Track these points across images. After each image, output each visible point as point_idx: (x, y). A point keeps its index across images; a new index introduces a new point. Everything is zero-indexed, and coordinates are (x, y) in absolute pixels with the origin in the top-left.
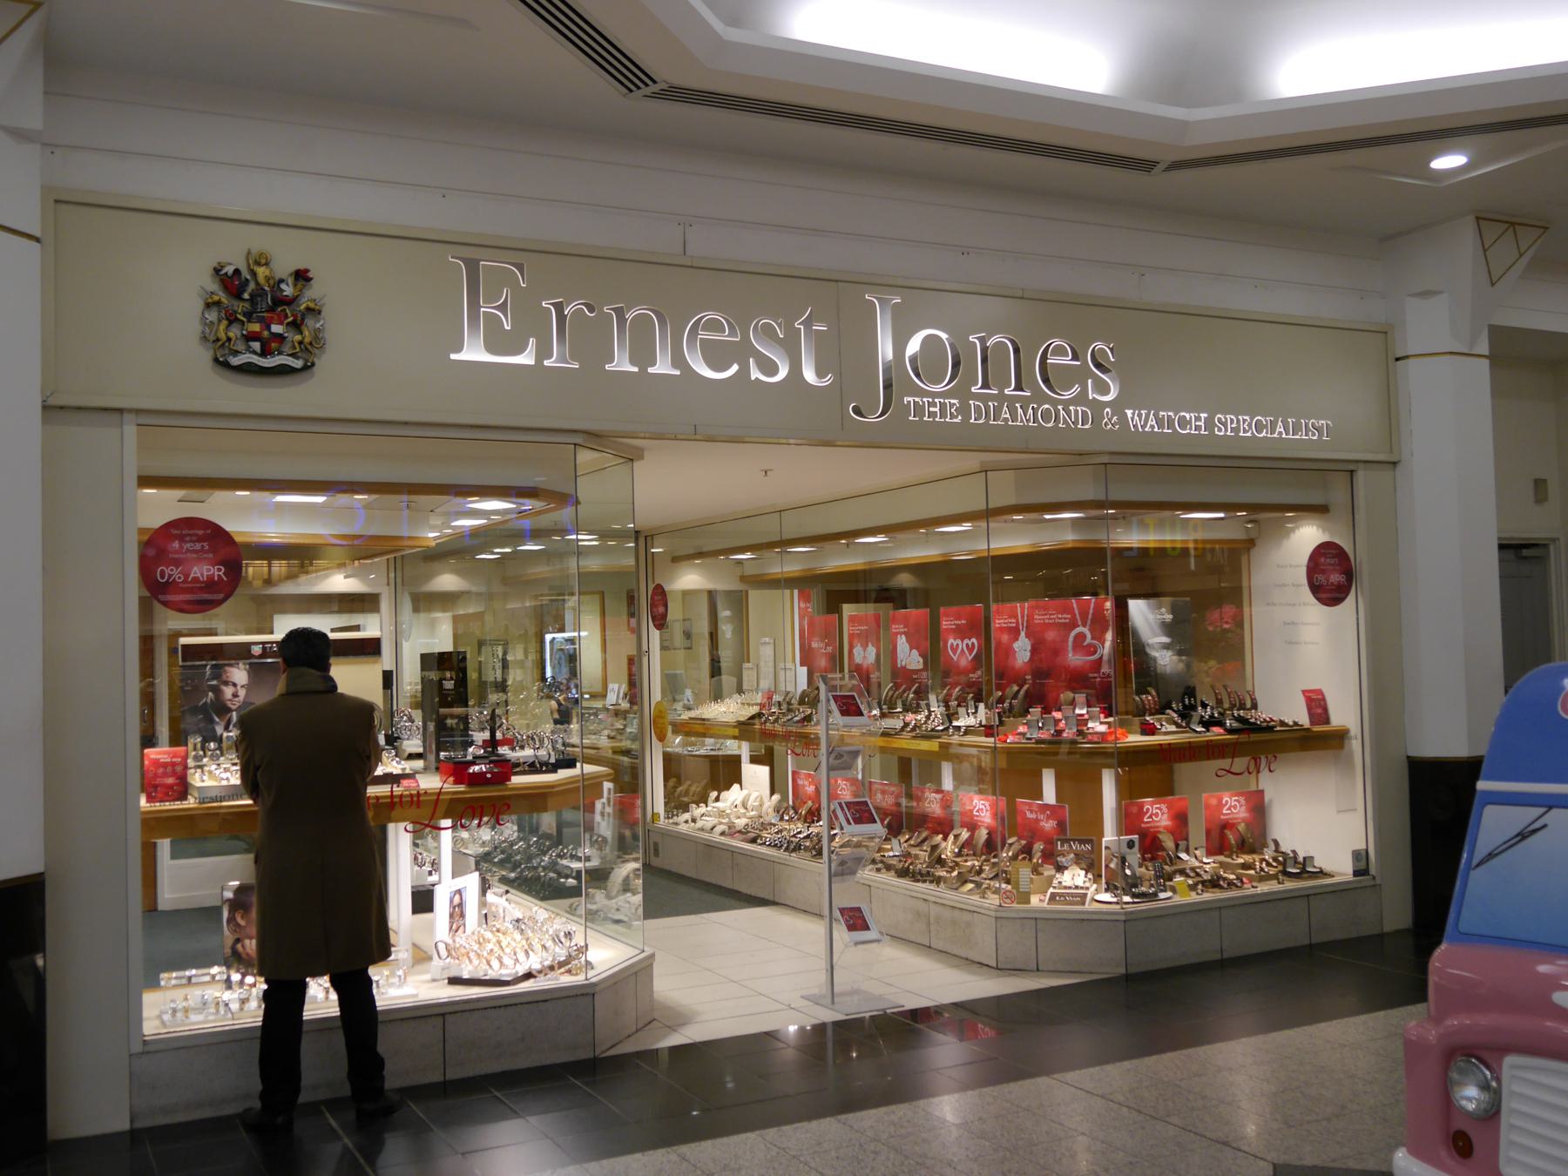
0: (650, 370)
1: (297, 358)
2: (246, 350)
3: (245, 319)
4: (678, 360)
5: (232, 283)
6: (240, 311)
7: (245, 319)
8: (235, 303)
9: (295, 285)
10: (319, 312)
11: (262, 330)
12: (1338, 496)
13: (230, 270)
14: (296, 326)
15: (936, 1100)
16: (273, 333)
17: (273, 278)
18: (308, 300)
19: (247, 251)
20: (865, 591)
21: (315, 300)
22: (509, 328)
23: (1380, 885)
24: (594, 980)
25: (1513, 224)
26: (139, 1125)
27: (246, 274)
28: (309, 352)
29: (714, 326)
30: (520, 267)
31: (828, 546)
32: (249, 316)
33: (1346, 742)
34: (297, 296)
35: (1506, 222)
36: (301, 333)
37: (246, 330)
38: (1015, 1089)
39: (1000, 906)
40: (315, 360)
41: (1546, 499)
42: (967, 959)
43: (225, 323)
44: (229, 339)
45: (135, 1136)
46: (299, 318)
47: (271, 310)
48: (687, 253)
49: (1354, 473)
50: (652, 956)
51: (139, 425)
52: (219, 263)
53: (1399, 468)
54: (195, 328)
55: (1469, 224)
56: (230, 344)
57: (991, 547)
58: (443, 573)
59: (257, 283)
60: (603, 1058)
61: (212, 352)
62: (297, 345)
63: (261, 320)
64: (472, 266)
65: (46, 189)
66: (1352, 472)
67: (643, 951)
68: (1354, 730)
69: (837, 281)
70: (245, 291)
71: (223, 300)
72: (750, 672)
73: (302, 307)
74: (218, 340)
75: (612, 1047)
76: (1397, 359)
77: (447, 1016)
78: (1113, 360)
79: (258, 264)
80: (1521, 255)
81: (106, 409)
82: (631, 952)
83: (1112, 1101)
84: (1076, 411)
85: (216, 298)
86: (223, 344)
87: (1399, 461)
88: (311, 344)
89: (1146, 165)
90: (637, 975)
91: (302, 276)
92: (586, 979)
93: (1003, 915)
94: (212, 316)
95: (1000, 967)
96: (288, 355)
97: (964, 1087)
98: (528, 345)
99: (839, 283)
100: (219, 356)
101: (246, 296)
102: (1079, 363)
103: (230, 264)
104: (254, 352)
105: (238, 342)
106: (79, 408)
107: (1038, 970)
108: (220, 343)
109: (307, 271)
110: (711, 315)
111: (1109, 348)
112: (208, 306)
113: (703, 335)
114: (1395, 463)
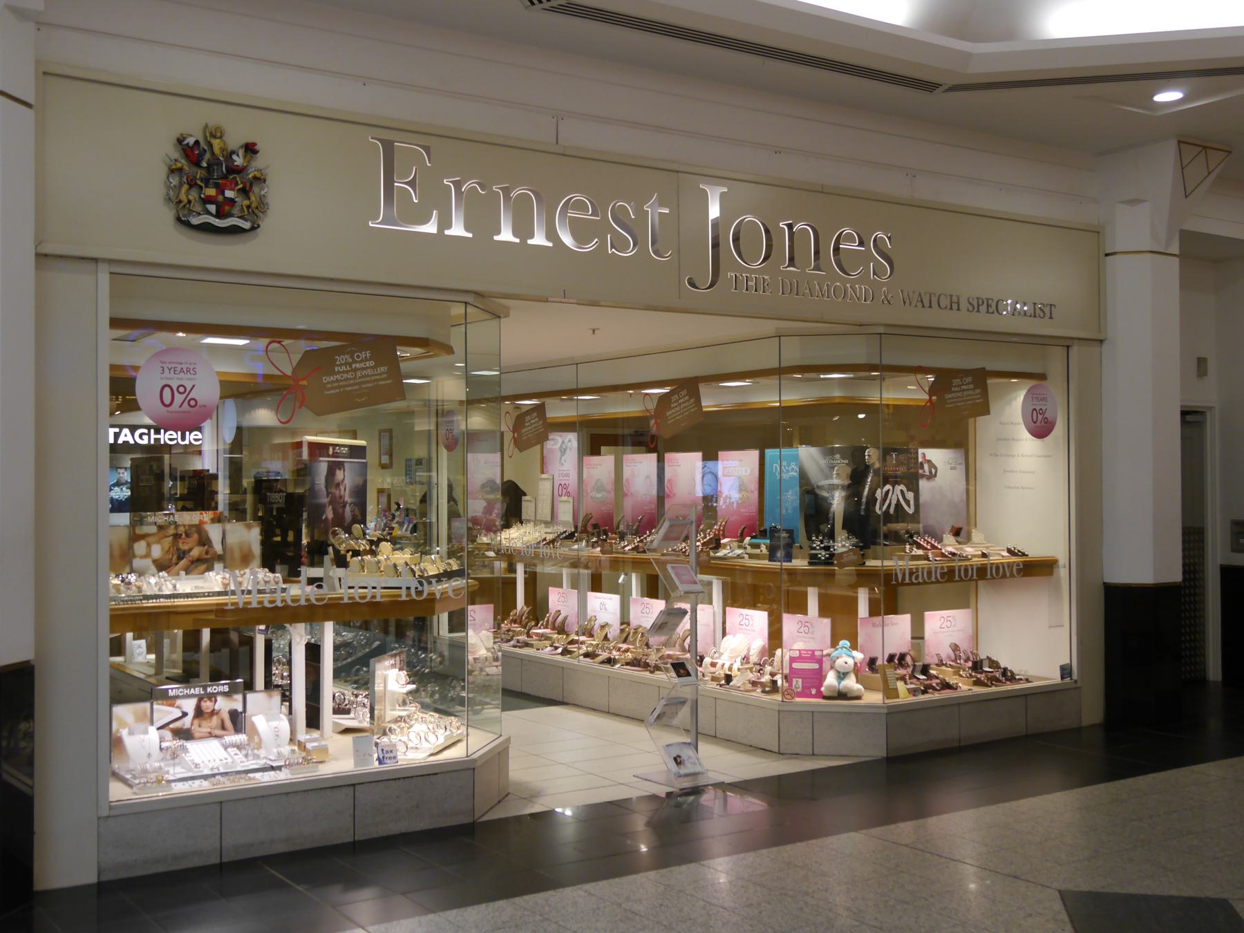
0: (530, 242)
1: (246, 220)
2: (203, 211)
3: (203, 185)
4: (552, 234)
5: (191, 152)
6: (198, 177)
7: (203, 185)
8: (195, 169)
9: (245, 157)
10: (265, 181)
11: (217, 193)
12: (1055, 367)
13: (191, 141)
14: (245, 192)
15: (712, 862)
16: (226, 198)
17: (227, 149)
18: (255, 171)
19: (204, 125)
20: (623, 435)
21: (261, 170)
22: (417, 201)
23: (1080, 688)
24: (475, 756)
25: (1205, 148)
26: (104, 878)
27: (203, 144)
28: (255, 213)
29: (580, 206)
30: (427, 149)
31: (611, 395)
32: (207, 182)
33: (1055, 570)
34: (247, 166)
35: (1200, 146)
36: (249, 199)
37: (204, 194)
38: (789, 850)
39: (783, 701)
40: (260, 223)
41: (1206, 374)
42: (751, 746)
43: (186, 187)
44: (189, 202)
45: (103, 888)
46: (248, 186)
47: (225, 177)
48: (560, 142)
49: (1070, 348)
50: (508, 740)
51: (111, 273)
52: (182, 135)
53: (1105, 345)
54: (162, 191)
55: (1172, 146)
56: (190, 205)
57: (782, 399)
58: (258, 407)
59: (213, 154)
60: (479, 822)
61: (174, 212)
62: (245, 208)
63: (217, 186)
64: (388, 146)
65: (38, 62)
66: (1068, 347)
67: (501, 736)
68: (1063, 560)
69: (677, 172)
70: (203, 159)
71: (186, 168)
72: (530, 503)
73: (250, 176)
74: (180, 202)
75: (483, 815)
76: (1107, 255)
77: (358, 787)
78: (890, 247)
79: (215, 137)
80: (1209, 173)
81: (83, 258)
82: (492, 737)
83: (915, 849)
84: (860, 288)
85: (179, 165)
86: (184, 206)
87: (1105, 339)
88: (257, 208)
89: (929, 86)
90: (499, 756)
91: (250, 149)
92: (467, 756)
93: (786, 708)
94: (174, 181)
95: (781, 752)
96: (238, 217)
97: (729, 854)
98: (432, 215)
99: (680, 174)
100: (181, 216)
101: (205, 165)
102: (863, 249)
103: (191, 136)
104: (209, 213)
105: (196, 203)
106: (61, 257)
107: (813, 754)
108: (182, 204)
109: (254, 144)
110: (578, 197)
111: (887, 237)
112: (172, 171)
113: (572, 214)
114: (1101, 341)
